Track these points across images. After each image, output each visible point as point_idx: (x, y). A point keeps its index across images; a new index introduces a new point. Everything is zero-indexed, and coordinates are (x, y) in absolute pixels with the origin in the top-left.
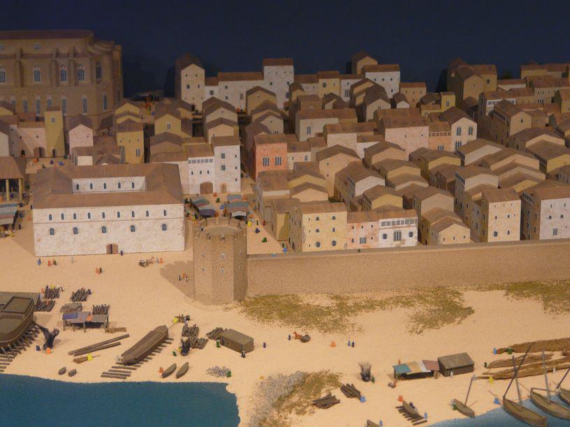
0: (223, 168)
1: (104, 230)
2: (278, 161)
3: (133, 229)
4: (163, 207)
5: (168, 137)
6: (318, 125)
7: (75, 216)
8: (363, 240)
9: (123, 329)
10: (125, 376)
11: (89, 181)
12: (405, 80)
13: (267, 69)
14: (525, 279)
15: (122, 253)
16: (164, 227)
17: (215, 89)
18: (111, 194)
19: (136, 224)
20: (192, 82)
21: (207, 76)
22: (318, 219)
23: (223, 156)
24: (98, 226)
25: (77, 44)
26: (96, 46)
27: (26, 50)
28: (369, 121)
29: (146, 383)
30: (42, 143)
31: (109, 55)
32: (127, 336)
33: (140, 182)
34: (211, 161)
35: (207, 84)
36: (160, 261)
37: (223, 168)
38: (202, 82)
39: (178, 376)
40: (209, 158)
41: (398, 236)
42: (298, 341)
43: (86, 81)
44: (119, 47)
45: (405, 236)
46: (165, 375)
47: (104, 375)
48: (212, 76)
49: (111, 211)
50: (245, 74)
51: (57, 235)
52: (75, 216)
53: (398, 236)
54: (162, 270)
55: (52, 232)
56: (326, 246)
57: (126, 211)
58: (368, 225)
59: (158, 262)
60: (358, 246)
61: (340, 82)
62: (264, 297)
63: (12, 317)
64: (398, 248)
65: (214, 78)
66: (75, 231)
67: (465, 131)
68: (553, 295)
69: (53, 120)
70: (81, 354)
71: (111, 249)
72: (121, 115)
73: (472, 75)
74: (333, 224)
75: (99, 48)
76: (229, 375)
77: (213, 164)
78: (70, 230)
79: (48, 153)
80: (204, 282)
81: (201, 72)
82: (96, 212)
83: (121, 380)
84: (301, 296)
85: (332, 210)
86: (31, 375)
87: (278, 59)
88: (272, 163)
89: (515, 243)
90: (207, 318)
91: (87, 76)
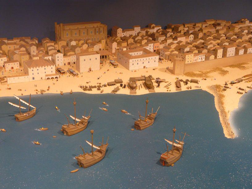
1: (143, 63)
3: (149, 62)
8: (196, 60)
14: (231, 64)
16: (155, 61)
17: (124, 33)
19: (149, 61)
20: (120, 31)
21: (123, 30)
23: (150, 46)
25: (99, 24)
30: (101, 48)
32: (240, 89)
33: (141, 52)
35: (123, 32)
41: (202, 59)
43: (102, 33)
44: (107, 26)
45: (203, 58)
46: (188, 89)
48: (123, 31)
49: (139, 59)
50: (128, 30)
53: (202, 59)
55: (133, 64)
56: (189, 62)
58: (197, 57)
60: (195, 61)
61: (30, 48)
64: (202, 61)
66: (138, 64)
67: (191, 37)
73: (72, 41)
74: (191, 57)
76: (238, 92)
78: (137, 64)
79: (102, 49)
80: (176, 71)
81: (122, 30)
82: (137, 59)
87: (137, 26)
89: (221, 58)
90: (185, 78)
91: (102, 32)
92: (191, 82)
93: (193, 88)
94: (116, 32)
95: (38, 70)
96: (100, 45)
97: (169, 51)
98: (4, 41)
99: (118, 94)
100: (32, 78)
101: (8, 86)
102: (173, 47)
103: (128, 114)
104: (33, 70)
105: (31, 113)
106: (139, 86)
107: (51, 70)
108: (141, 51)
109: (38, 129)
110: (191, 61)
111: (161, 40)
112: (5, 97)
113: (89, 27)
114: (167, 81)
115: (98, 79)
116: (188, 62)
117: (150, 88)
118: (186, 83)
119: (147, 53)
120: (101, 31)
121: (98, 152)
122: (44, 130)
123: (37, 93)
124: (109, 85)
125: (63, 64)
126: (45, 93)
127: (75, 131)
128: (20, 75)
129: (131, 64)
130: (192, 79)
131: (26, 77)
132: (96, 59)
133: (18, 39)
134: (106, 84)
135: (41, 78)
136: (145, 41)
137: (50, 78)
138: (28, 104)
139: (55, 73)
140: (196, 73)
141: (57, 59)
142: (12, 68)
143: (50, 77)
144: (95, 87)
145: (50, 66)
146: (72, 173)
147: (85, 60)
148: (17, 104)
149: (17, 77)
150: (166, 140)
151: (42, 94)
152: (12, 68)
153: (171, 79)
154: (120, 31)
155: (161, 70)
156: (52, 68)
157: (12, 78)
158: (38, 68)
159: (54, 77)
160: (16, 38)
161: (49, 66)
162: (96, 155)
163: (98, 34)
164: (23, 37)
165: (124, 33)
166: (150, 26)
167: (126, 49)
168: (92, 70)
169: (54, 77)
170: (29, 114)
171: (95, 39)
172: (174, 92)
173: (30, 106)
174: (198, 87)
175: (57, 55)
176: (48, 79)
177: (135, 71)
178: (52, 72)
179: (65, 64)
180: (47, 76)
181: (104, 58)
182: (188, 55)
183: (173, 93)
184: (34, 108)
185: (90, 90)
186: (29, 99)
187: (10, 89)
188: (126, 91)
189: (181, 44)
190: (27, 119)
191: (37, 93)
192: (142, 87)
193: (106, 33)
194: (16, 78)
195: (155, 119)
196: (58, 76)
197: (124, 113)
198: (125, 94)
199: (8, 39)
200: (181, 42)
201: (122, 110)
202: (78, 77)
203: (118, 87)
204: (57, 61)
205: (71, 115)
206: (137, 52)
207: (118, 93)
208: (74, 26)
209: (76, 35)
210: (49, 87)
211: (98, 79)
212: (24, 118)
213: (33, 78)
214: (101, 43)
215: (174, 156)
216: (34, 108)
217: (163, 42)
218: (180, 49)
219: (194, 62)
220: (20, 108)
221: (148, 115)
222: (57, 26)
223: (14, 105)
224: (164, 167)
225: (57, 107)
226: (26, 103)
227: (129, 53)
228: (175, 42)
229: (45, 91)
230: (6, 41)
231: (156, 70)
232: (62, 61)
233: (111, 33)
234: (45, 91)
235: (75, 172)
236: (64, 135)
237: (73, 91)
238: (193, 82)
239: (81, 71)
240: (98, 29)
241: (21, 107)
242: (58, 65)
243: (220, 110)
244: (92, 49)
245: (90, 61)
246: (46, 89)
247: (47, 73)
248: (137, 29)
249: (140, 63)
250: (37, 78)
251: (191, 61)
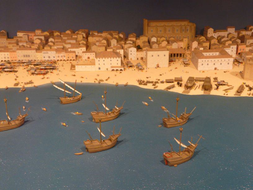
0: (232, 51)
1: (214, 64)
2: (243, 50)
3: (221, 64)
5: (215, 44)
7: (208, 61)
10: (240, 95)
11: (206, 53)
15: (218, 70)
16: (228, 64)
18: (214, 56)
19: (222, 63)
23: (232, 48)
24: (213, 63)
27: (158, 25)
29: (245, 97)
30: (182, 46)
31: (194, 26)
33: (218, 54)
35: (214, 33)
37: (232, 51)
38: (213, 32)
43: (189, 32)
47: (234, 95)
48: (215, 32)
49: (210, 60)
51: (203, 65)
52: (208, 61)
55: (202, 64)
57: (213, 60)
66: (208, 64)
77: (230, 50)
80: (246, 75)
82: (207, 60)
86: (217, 95)
88: (7, 58)
91: (189, 31)
94: (207, 32)
96: (182, 43)
98: (94, 33)
99: (158, 90)
100: (98, 68)
101: (75, 73)
103: (167, 111)
105: (76, 98)
107: (116, 62)
108: (216, 52)
109: (74, 113)
112: (132, 85)
115: (161, 75)
117: (206, 90)
120: (188, 29)
121: (109, 141)
122: (78, 115)
123: (95, 82)
124: (166, 82)
125: (136, 59)
126: (103, 82)
127: (171, 125)
129: (200, 64)
131: (93, 66)
132: (165, 55)
133: (107, 32)
134: (165, 81)
135: (107, 69)
136: (230, 42)
138: (73, 89)
141: (130, 53)
142: (89, 58)
144: (152, 82)
145: (116, 58)
146: (76, 155)
147: (152, 56)
148: (62, 88)
149: (85, 66)
150: (175, 139)
152: (89, 58)
155: (232, 73)
156: (104, 61)
158: (104, 59)
159: (119, 69)
160: (106, 32)
162: (106, 143)
163: (184, 32)
165: (215, 34)
166: (248, 28)
168: (159, 66)
170: (74, 99)
173: (76, 91)
175: (130, 49)
176: (113, 70)
178: (117, 64)
180: (112, 67)
184: (80, 94)
185: (146, 84)
186: (75, 85)
187: (74, 75)
194: (84, 67)
195: (189, 119)
196: (123, 69)
197: (163, 110)
198: (177, 93)
199: (98, 33)
201: (162, 107)
205: (104, 104)
207: (171, 90)
208: (160, 23)
211: (161, 75)
212: (68, 102)
213: (99, 68)
214: (183, 42)
215: (180, 156)
216: (80, 93)
221: (182, 114)
223: (59, 88)
224: (165, 166)
226: (71, 88)
227: (203, 53)
229: (103, 81)
230: (96, 34)
234: (103, 81)
235: (80, 155)
236: (92, 121)
237: (129, 84)
239: (148, 66)
241: (66, 91)
242: (131, 59)
244: (170, 46)
245: (158, 57)
248: (232, 30)
249: (211, 64)
250: (103, 69)
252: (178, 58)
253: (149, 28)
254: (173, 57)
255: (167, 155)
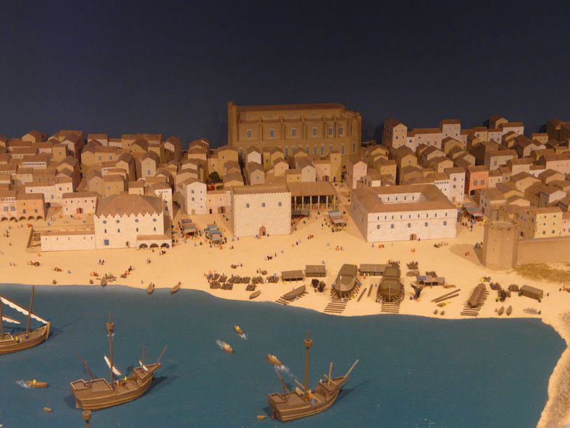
0: (455, 187)
1: (409, 225)
2: (483, 182)
3: (426, 224)
4: (446, 211)
5: (410, 169)
6: (502, 160)
9: (453, 286)
12: (467, 127)
13: (445, 126)
16: (445, 223)
19: (428, 221)
20: (399, 132)
22: (545, 217)
23: (455, 180)
25: (337, 113)
26: (346, 113)
27: (286, 118)
28: (525, 157)
30: (327, 173)
31: (356, 120)
33: (417, 196)
34: (448, 182)
35: (408, 136)
36: (447, 244)
37: (455, 187)
39: (508, 314)
40: (446, 181)
42: (566, 292)
46: (500, 314)
47: (462, 314)
48: (410, 133)
49: (397, 214)
50: (423, 129)
51: (381, 229)
54: (313, 280)
56: (549, 234)
57: (406, 214)
59: (445, 245)
62: (527, 265)
63: (390, 280)
65: (412, 132)
66: (392, 226)
68: (337, 410)
69: (336, 159)
70: (439, 301)
71: (413, 237)
72: (376, 155)
75: (349, 115)
79: (331, 179)
80: (491, 256)
81: (405, 128)
82: (389, 215)
83: (475, 317)
84: (549, 264)
85: (553, 211)
87: (451, 119)
90: (507, 279)
92: (520, 295)
93: (518, 313)
95: (118, 222)
96: (327, 166)
97: (503, 198)
100: (103, 241)
102: (523, 185)
103: (283, 367)
104: (105, 222)
105: (35, 335)
106: (366, 289)
107: (152, 224)
110: (553, 232)
111: (499, 164)
113: (310, 117)
114: (449, 284)
115: (270, 258)
116: (544, 233)
118: (503, 296)
119: (434, 199)
122: (37, 387)
126: (114, 283)
127: (104, 400)
128: (88, 230)
129: (371, 227)
130: (525, 286)
132: (280, 204)
134: (279, 275)
137: (149, 245)
138: (26, 313)
139: (163, 233)
140: (556, 267)
141: (189, 196)
142: (80, 211)
143: (149, 243)
147: (248, 206)
151: (104, 285)
153: (466, 276)
154: (399, 132)
155: (456, 250)
157: (53, 238)
158: (117, 217)
159: (160, 243)
161: (147, 215)
164: (145, 135)
165: (410, 138)
166: (494, 123)
167: (379, 182)
168: (267, 232)
169: (160, 243)
171: (343, 147)
172: (457, 318)
173: (33, 316)
174: (532, 311)
177: (380, 247)
179: (211, 211)
180: (140, 238)
181: (325, 202)
182: (543, 215)
183: (455, 320)
184: (45, 325)
188: (316, 302)
189: (549, 180)
190: (20, 350)
191: (91, 282)
192: (369, 295)
193: (356, 134)
194: (63, 238)
196: (169, 242)
197: (273, 364)
200: (552, 173)
202: (221, 248)
203: (304, 287)
204: (189, 201)
205: (108, 357)
206: (403, 195)
207: (296, 304)
209: (315, 134)
210: (130, 270)
211: (270, 258)
213: (107, 242)
216: (44, 322)
217: (500, 172)
218: (538, 195)
219: (562, 235)
220: (29, 316)
222: (233, 110)
225: (238, 328)
226: (19, 309)
228: (537, 172)
230: (104, 142)
231: (441, 248)
232: (203, 203)
233: (374, 135)
237: (182, 287)
238: (526, 295)
240: (331, 123)
242: (193, 211)
243: (559, 391)
244: (297, 176)
246: (117, 274)
247: (142, 232)
248: (452, 130)
249: (401, 226)
251: (553, 232)
252: (316, 208)
253: (242, 126)
254: (302, 206)
255: (277, 399)
